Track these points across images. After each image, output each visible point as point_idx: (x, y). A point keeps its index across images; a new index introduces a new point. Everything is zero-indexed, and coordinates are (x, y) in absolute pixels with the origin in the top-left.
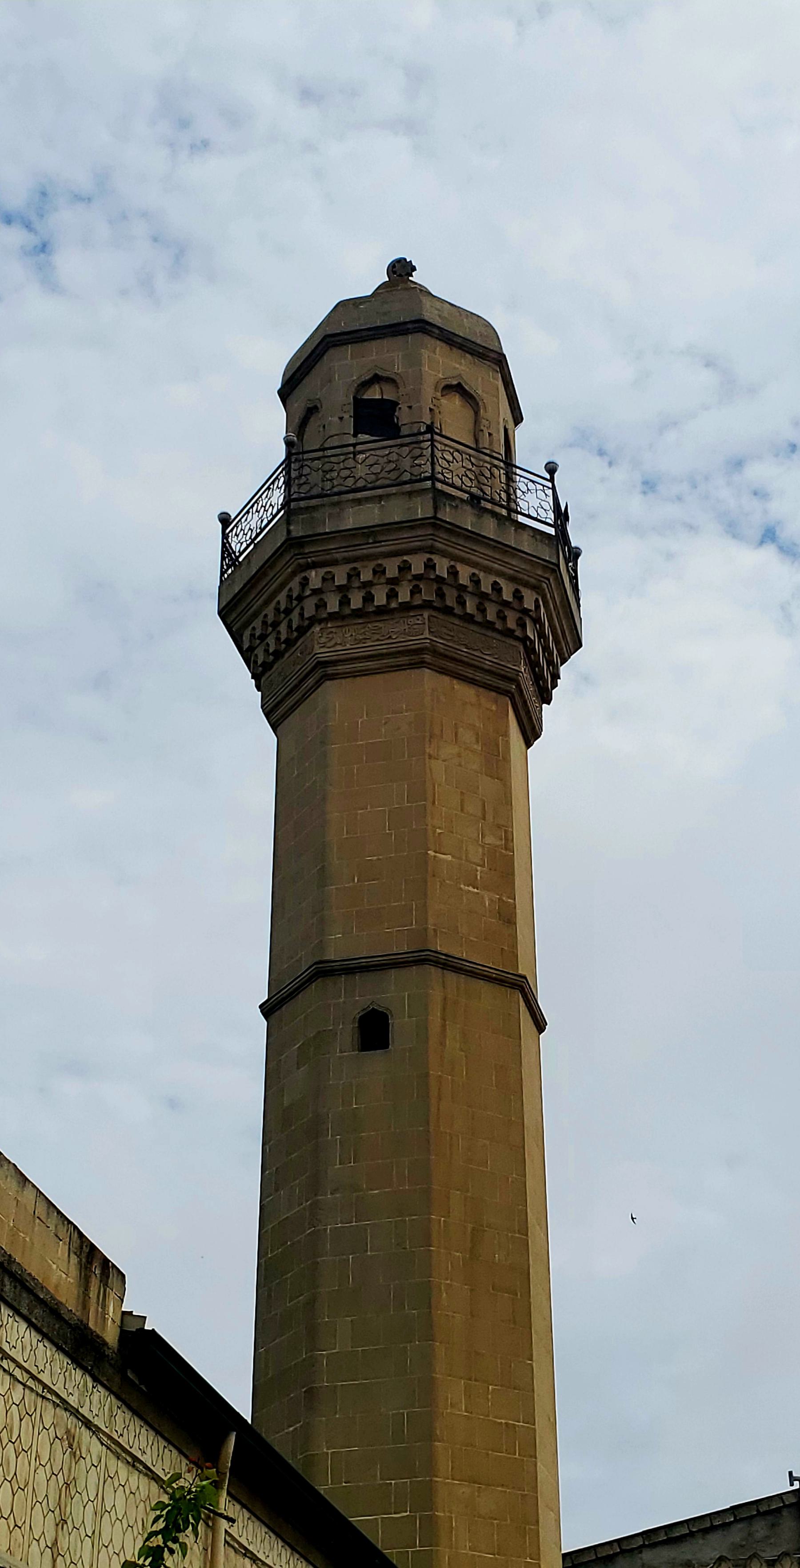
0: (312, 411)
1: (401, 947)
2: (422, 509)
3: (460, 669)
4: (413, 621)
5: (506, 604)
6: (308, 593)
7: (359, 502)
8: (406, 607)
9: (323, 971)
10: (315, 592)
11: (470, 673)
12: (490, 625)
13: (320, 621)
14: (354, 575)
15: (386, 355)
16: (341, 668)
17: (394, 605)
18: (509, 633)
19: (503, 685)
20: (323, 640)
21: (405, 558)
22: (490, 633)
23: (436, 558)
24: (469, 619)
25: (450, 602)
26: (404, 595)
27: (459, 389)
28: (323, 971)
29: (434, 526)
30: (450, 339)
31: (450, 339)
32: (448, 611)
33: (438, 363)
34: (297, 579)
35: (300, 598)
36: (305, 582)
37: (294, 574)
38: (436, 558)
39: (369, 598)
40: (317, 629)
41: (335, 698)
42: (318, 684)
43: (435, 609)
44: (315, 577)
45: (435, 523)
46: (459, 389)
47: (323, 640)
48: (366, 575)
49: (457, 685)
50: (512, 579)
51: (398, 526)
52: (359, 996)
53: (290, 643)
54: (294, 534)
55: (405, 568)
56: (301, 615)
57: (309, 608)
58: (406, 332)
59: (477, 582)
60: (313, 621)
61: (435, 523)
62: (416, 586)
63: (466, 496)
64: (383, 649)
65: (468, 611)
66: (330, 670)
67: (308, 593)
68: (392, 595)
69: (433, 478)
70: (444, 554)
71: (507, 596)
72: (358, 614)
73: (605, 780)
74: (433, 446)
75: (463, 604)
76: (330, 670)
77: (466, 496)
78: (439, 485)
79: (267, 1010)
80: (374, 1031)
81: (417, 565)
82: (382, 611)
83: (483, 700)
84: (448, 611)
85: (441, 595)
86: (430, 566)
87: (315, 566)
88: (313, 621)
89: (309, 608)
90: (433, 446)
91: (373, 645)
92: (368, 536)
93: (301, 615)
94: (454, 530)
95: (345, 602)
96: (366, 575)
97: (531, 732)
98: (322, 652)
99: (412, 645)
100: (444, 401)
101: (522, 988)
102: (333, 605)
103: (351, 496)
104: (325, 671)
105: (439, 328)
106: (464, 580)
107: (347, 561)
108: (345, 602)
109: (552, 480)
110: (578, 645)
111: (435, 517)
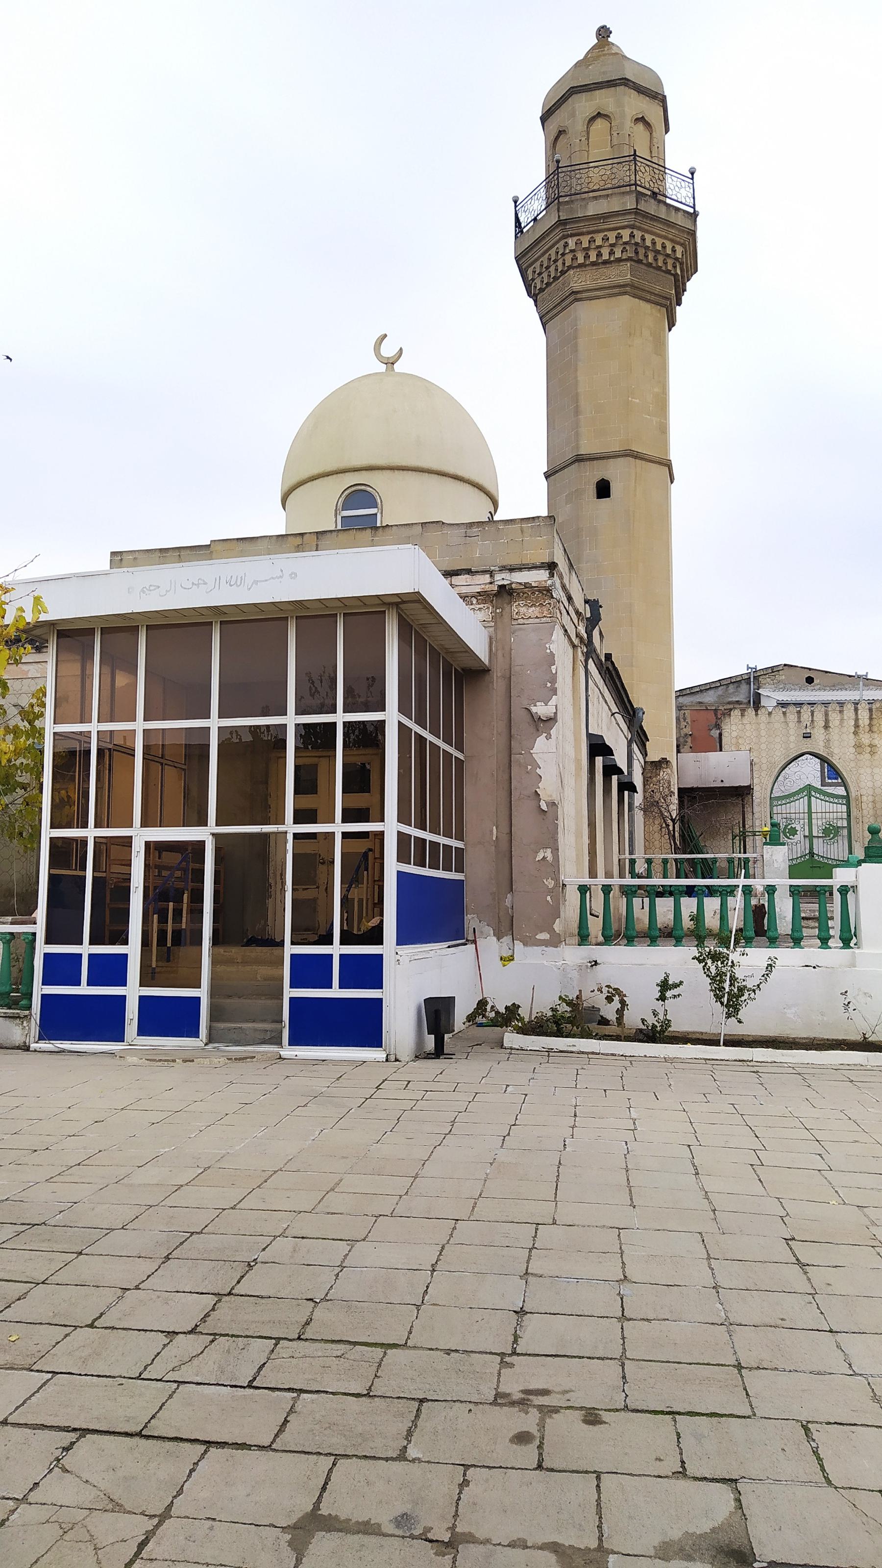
0: (561, 133)
1: (616, 448)
2: (630, 203)
3: (644, 294)
4: (621, 268)
5: (668, 256)
6: (567, 251)
7: (595, 198)
8: (619, 260)
9: (579, 459)
10: (572, 251)
11: (648, 296)
12: (659, 268)
13: (574, 268)
14: (591, 241)
15: (604, 100)
16: (584, 295)
17: (612, 259)
18: (668, 272)
19: (663, 301)
20: (576, 279)
21: (619, 231)
22: (658, 272)
23: (635, 232)
24: (649, 265)
25: (641, 257)
26: (618, 255)
27: (642, 120)
28: (579, 459)
29: (636, 213)
30: (641, 90)
31: (641, 90)
32: (639, 261)
33: (635, 104)
34: (562, 242)
35: (563, 255)
36: (566, 245)
37: (560, 239)
38: (635, 232)
39: (599, 255)
40: (571, 272)
41: (586, 314)
42: (571, 303)
43: (634, 261)
44: (571, 242)
45: (637, 212)
46: (642, 120)
47: (576, 279)
48: (599, 242)
49: (642, 303)
50: (672, 241)
51: (616, 214)
52: (594, 473)
53: (556, 278)
54: (561, 218)
55: (619, 237)
56: (564, 264)
57: (568, 258)
58: (615, 85)
59: (654, 243)
60: (569, 268)
61: (637, 212)
62: (624, 248)
63: (649, 193)
64: (606, 283)
65: (650, 261)
66: (579, 296)
67: (567, 251)
68: (611, 253)
69: (636, 185)
70: (639, 229)
71: (669, 251)
72: (594, 264)
73: (709, 349)
74: (636, 164)
75: (646, 257)
76: (579, 296)
77: (649, 193)
78: (638, 188)
79: (547, 476)
80: (603, 490)
81: (626, 234)
82: (605, 262)
83: (654, 311)
84: (639, 261)
85: (637, 253)
86: (632, 236)
87: (572, 235)
88: (569, 268)
89: (568, 258)
90: (636, 164)
91: (602, 282)
92: (600, 219)
93: (564, 264)
94: (646, 215)
95: (587, 257)
96: (599, 242)
97: (672, 324)
98: (576, 286)
99: (621, 282)
100: (635, 127)
101: (668, 465)
102: (581, 260)
103: (591, 194)
104: (576, 296)
105: (633, 82)
106: (648, 243)
107: (589, 233)
108: (587, 257)
109: (692, 179)
110: (696, 271)
111: (637, 209)
